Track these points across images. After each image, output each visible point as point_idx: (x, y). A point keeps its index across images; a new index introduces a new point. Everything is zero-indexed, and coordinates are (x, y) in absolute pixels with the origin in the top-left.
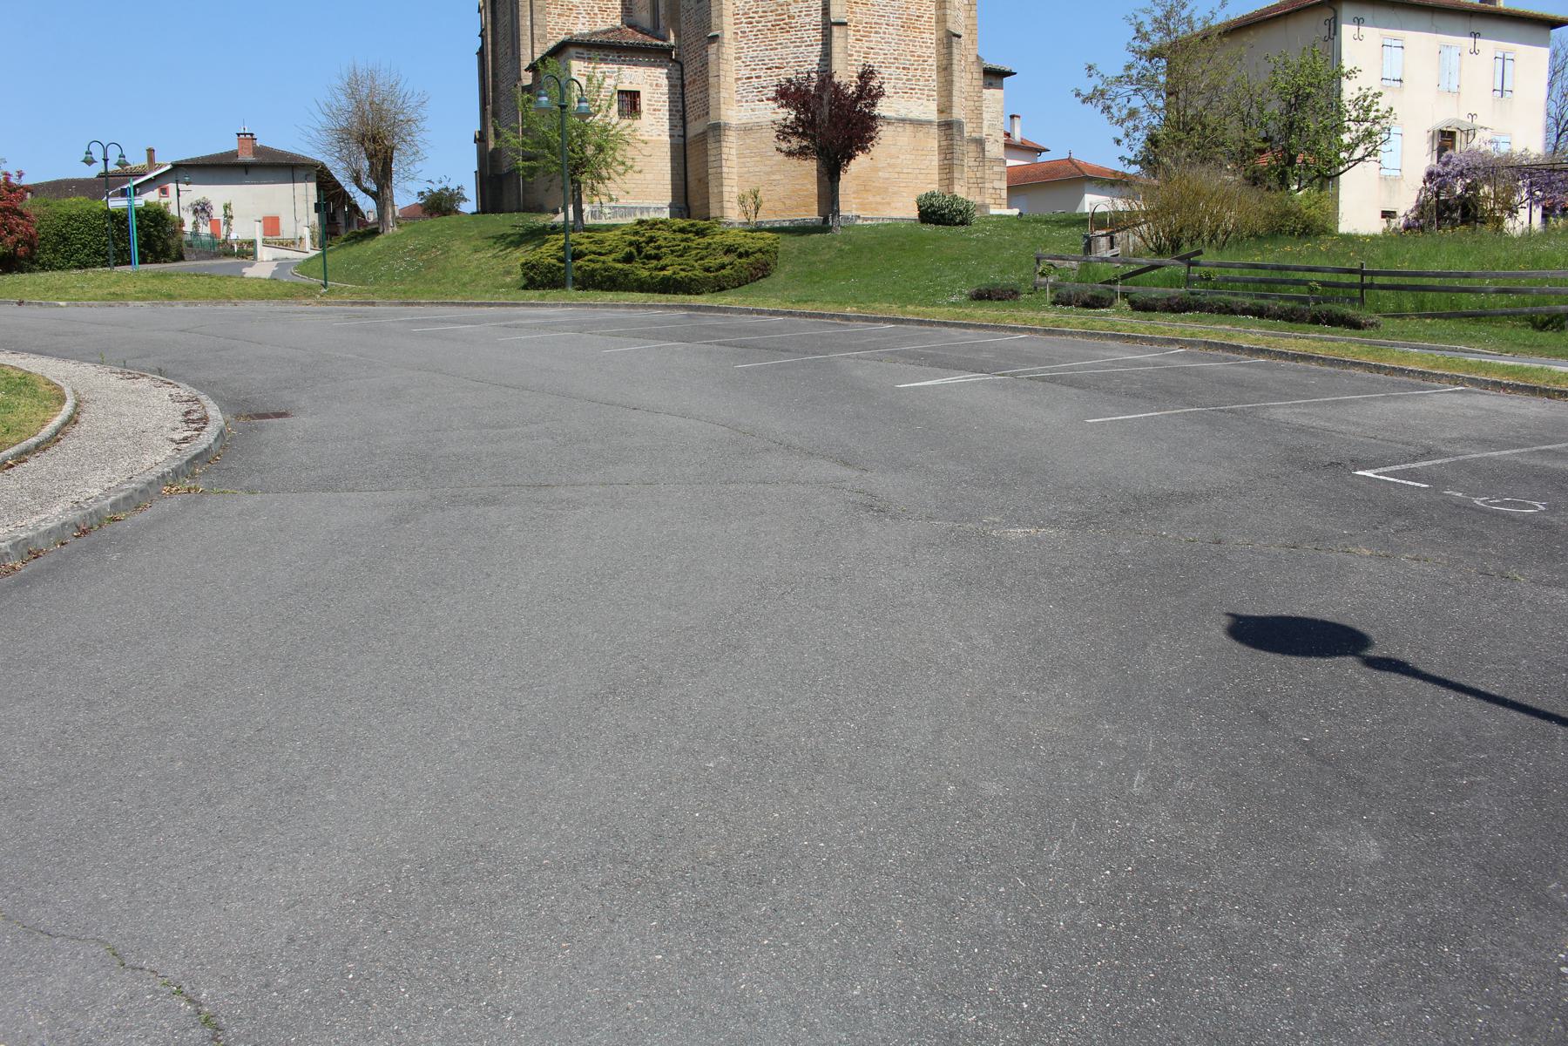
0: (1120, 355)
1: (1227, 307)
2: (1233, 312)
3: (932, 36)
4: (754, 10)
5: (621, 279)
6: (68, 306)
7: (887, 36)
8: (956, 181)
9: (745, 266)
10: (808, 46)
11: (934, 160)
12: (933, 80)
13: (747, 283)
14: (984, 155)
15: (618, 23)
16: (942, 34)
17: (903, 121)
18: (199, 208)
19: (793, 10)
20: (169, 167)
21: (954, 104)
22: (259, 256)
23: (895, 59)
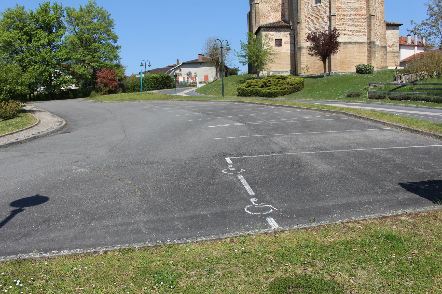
0: (303, 116)
1: (417, 98)
2: (419, 100)
3: (365, 16)
4: (310, 13)
5: (259, 92)
6: (109, 103)
7: (350, 18)
8: (372, 60)
9: (291, 88)
10: (326, 23)
11: (366, 54)
12: (366, 30)
13: (292, 93)
14: (386, 51)
15: (280, 20)
16: (368, 15)
17: (355, 43)
18: (189, 74)
19: (321, 13)
20: (181, 64)
21: (372, 36)
22: (198, 86)
23: (352, 24)
